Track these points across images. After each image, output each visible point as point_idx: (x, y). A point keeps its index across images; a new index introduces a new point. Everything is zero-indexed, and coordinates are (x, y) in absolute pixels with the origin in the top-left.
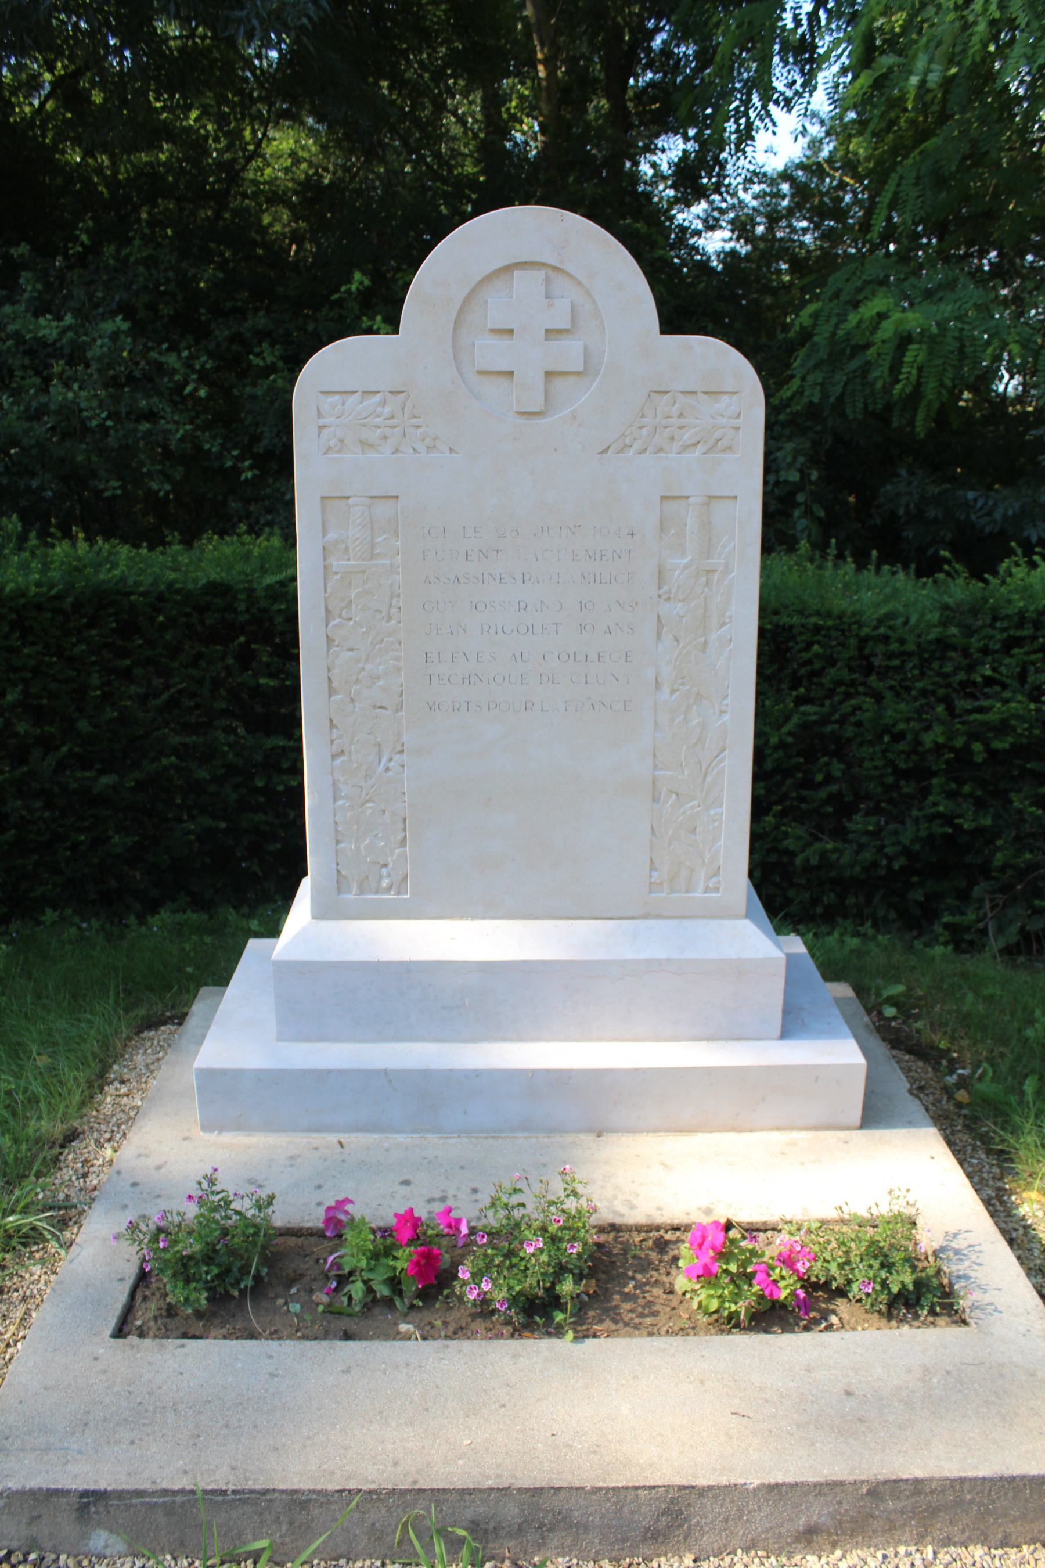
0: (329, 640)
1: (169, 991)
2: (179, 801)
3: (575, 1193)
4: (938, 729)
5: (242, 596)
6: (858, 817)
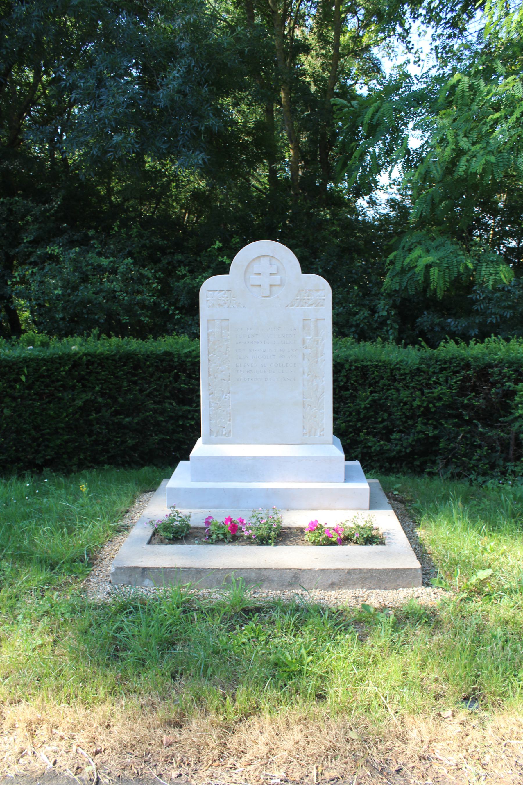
0: (209, 360)
1: (151, 486)
4: (418, 399)
5: (176, 356)
6: (394, 434)
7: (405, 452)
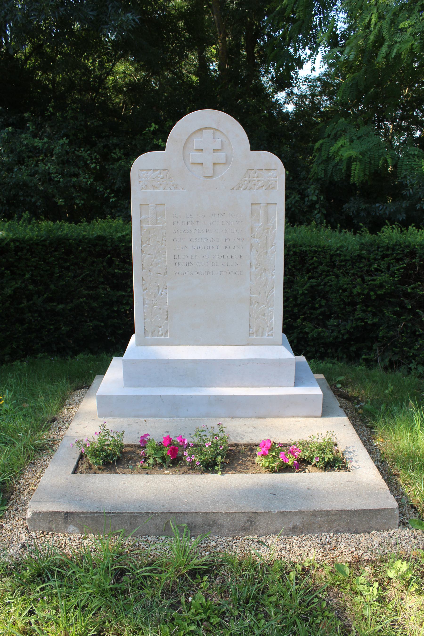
1: (83, 380)
2: (86, 315)
3: (222, 431)
4: (358, 287)
5: (109, 241)
6: (331, 320)
7: (342, 338)
